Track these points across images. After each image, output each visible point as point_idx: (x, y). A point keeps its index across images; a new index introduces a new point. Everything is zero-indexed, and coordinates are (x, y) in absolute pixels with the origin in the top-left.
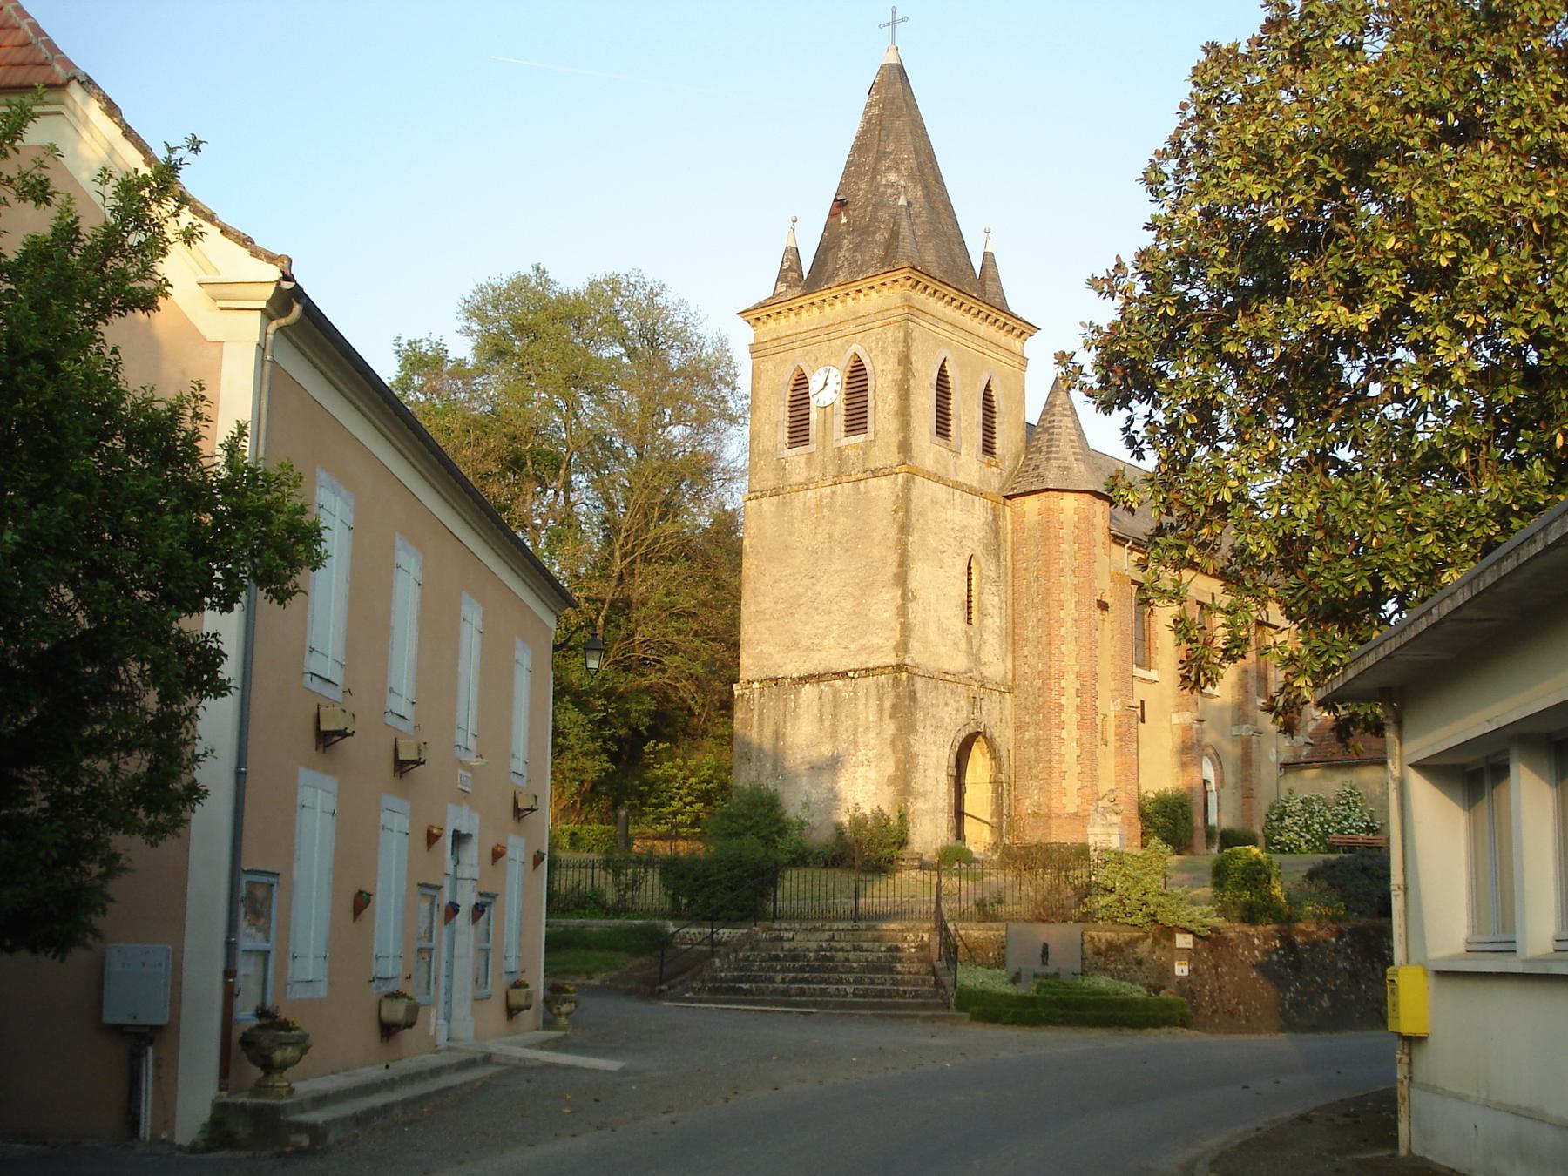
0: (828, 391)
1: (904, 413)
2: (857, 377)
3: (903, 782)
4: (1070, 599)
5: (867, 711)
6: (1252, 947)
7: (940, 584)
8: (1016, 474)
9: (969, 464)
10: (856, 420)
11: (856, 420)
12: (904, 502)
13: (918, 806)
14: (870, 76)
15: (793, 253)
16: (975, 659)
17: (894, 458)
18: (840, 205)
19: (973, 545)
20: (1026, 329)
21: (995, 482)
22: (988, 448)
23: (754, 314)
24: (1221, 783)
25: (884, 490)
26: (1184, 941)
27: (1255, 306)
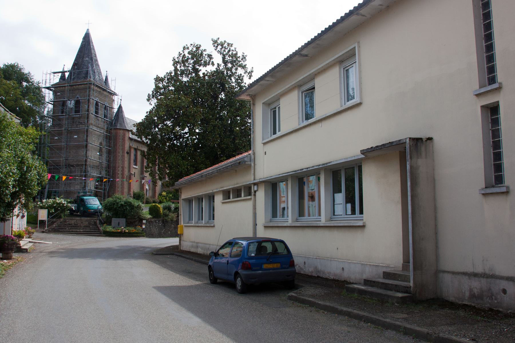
4: (121, 151)
6: (156, 223)
24: (149, 189)
26: (144, 221)
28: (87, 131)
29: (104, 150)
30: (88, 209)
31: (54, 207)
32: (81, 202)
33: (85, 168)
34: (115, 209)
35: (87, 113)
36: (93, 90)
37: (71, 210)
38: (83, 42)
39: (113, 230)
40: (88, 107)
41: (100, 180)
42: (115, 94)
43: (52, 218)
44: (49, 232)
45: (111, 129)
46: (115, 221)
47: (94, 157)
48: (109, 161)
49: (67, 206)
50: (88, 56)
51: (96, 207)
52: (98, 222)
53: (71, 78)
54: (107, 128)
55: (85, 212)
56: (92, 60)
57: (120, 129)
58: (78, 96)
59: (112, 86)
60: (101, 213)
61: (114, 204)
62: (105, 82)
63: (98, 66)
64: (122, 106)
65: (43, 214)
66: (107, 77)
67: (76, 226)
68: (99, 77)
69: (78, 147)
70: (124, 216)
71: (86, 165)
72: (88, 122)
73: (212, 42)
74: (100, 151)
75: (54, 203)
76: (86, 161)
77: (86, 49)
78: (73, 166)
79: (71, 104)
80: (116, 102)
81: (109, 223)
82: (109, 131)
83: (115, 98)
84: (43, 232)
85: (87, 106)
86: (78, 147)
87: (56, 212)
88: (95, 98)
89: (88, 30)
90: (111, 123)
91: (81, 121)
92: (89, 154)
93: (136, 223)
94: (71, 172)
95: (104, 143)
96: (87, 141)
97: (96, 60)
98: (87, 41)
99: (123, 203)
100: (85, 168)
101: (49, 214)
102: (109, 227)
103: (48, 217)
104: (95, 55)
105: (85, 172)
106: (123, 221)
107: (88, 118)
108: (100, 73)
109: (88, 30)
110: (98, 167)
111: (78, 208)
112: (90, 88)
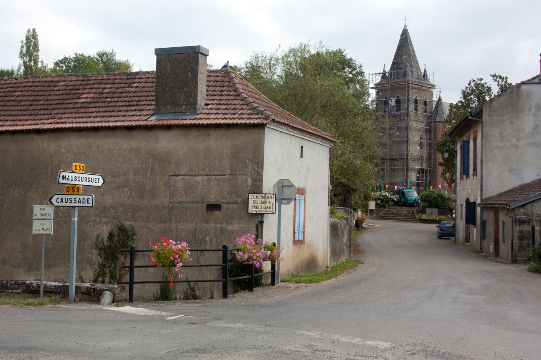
18: (393, 64)
28: (407, 127)
29: (425, 143)
30: (408, 200)
31: (380, 199)
32: (402, 194)
33: (407, 162)
34: (429, 201)
35: (406, 111)
36: (412, 88)
37: (394, 201)
38: (400, 39)
39: (427, 218)
40: (408, 105)
41: (421, 171)
42: (434, 86)
43: (379, 207)
44: (377, 218)
45: (430, 123)
46: (428, 210)
47: (415, 151)
48: (429, 153)
49: (390, 198)
50: (406, 53)
51: (414, 198)
52: (415, 211)
53: (391, 77)
54: (427, 122)
55: (405, 202)
56: (410, 57)
57: (440, 122)
58: (398, 95)
59: (431, 79)
60: (418, 204)
61: (428, 197)
62: (424, 77)
63: (417, 61)
64: (442, 98)
65: (372, 205)
66: (425, 70)
67: (397, 214)
68: (418, 73)
69: (400, 142)
70: (437, 207)
71: (407, 159)
72: (408, 119)
73: (492, 78)
74: (421, 145)
75: (380, 195)
76: (407, 155)
77: (405, 44)
78: (396, 159)
79: (392, 103)
80: (435, 96)
81: (423, 212)
82: (429, 124)
83: (434, 91)
84: (373, 219)
85: (406, 105)
86: (400, 142)
87: (382, 203)
88: (413, 95)
89: (405, 26)
90: (431, 116)
91: (402, 118)
92: (410, 148)
93: (448, 213)
94: (394, 166)
95: (424, 137)
96: (408, 137)
97: (415, 56)
98: (405, 37)
99: (435, 196)
100: (407, 162)
101: (376, 204)
102: (424, 215)
103: (376, 207)
104: (413, 50)
105: (407, 165)
106: (436, 211)
107: (408, 116)
108: (418, 68)
109: (405, 26)
110: (421, 159)
111: (400, 198)
112: (408, 87)
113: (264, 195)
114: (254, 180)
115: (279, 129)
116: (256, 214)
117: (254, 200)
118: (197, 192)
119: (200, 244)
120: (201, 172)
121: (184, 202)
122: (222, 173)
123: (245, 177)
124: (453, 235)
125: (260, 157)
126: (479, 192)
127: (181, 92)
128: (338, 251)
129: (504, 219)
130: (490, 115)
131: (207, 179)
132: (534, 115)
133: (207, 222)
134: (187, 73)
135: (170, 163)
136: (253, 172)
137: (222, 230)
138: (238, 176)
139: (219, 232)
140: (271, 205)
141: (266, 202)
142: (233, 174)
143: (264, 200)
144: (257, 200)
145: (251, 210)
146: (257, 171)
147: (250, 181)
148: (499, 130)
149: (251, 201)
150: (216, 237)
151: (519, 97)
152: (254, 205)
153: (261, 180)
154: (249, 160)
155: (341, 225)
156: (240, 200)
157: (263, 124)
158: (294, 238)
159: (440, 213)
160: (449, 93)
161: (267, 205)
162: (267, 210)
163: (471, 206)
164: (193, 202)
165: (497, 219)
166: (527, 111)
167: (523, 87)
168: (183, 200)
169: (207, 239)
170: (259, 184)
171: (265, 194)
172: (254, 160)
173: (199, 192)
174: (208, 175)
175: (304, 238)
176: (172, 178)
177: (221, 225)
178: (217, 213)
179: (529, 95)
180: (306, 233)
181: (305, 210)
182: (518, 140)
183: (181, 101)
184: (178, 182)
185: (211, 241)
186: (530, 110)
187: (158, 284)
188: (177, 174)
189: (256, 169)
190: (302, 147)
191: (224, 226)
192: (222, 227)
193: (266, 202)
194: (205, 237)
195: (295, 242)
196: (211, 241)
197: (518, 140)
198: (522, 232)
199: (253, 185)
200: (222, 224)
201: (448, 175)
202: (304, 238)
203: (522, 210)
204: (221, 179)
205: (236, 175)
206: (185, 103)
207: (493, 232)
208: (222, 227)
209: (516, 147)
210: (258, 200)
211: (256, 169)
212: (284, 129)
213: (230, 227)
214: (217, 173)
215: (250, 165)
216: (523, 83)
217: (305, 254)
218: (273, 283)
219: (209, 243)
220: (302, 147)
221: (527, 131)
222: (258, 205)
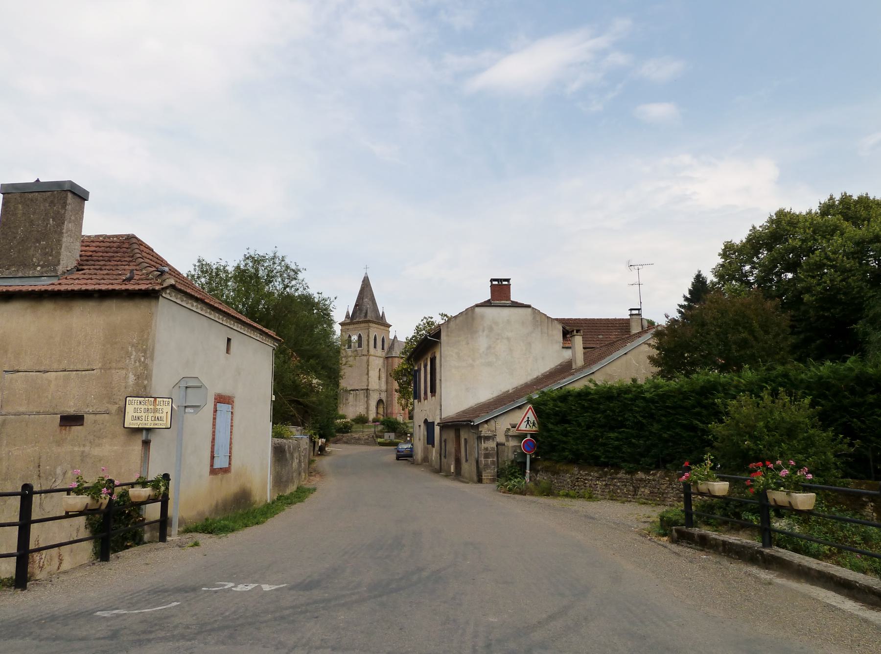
0: (355, 338)
1: (368, 345)
2: (360, 337)
3: (367, 409)
5: (362, 396)
7: (374, 374)
8: (387, 353)
9: (379, 352)
10: (360, 346)
11: (360, 346)
12: (368, 361)
13: (370, 412)
14: (52, 173)
15: (348, 313)
16: (380, 386)
17: (366, 353)
18: (356, 306)
19: (380, 367)
20: (389, 326)
21: (384, 354)
22: (383, 349)
23: (342, 324)
25: (365, 358)
27: (686, 464)
98: (366, 285)
113: (152, 399)
114: (138, 377)
115: (189, 306)
116: (139, 430)
117: (136, 406)
118: (47, 397)
119: (47, 479)
120: (55, 366)
121: (24, 414)
122: (89, 367)
123: (124, 372)
124: (411, 456)
125: (150, 341)
126: (438, 412)
127: (35, 247)
128: (284, 479)
129: (466, 437)
130: (448, 336)
131: (64, 376)
132: (487, 336)
133: (59, 444)
134: (49, 220)
135: (6, 352)
136: (137, 364)
137: (84, 456)
138: (113, 371)
139: (78, 458)
140: (164, 415)
141: (155, 411)
142: (106, 368)
143: (152, 407)
144: (140, 406)
145: (130, 423)
146: (143, 362)
147: (132, 378)
148: (456, 350)
149: (130, 409)
150: (73, 468)
151: (473, 319)
152: (135, 415)
153: (149, 377)
154: (133, 346)
155: (289, 447)
156: (114, 408)
157: (154, 290)
158: (212, 465)
159: (397, 437)
160: (403, 328)
161: (157, 415)
162: (157, 422)
163: (429, 426)
164: (38, 413)
165: (458, 438)
166: (480, 333)
167: (477, 309)
168: (22, 409)
169: (59, 471)
170: (146, 382)
171: (155, 398)
172: (140, 346)
173: (50, 397)
174: (65, 371)
175: (230, 464)
176: (8, 376)
177: (82, 449)
178: (76, 429)
179: (482, 317)
180: (233, 458)
181: (232, 426)
182: (474, 360)
183: (34, 260)
184: (17, 381)
185: (64, 474)
186: (483, 331)
187: (82, 520)
188: (16, 368)
189: (142, 359)
190: (229, 340)
191: (87, 449)
192: (83, 452)
193: (155, 411)
194: (55, 468)
195: (213, 471)
196: (64, 474)
197: (474, 360)
198: (486, 449)
199: (137, 384)
200: (84, 446)
201: (403, 402)
202: (230, 464)
203: (486, 426)
204: (86, 375)
205: (110, 368)
206: (41, 263)
207: (453, 450)
208: (83, 452)
209: (472, 366)
210: (143, 407)
211: (142, 359)
212: (195, 306)
213: (96, 451)
214: (79, 367)
215: (134, 353)
216: (477, 306)
217: (229, 487)
218: (163, 538)
219: (61, 478)
220: (229, 340)
221: (481, 351)
222: (143, 414)
